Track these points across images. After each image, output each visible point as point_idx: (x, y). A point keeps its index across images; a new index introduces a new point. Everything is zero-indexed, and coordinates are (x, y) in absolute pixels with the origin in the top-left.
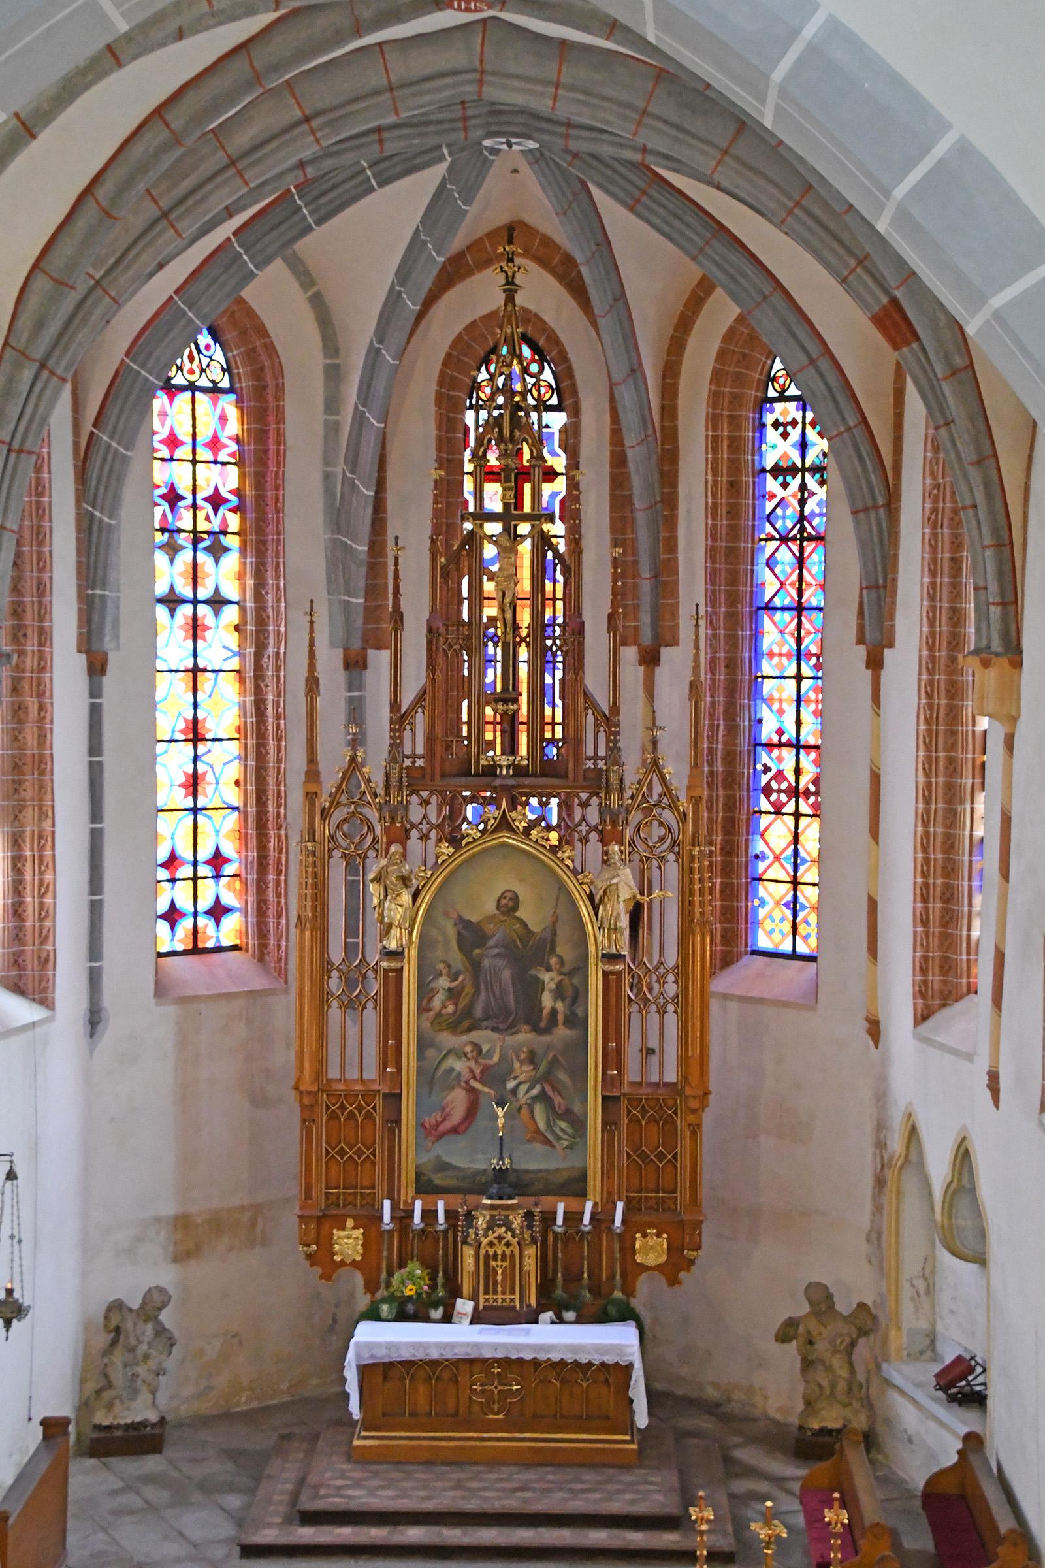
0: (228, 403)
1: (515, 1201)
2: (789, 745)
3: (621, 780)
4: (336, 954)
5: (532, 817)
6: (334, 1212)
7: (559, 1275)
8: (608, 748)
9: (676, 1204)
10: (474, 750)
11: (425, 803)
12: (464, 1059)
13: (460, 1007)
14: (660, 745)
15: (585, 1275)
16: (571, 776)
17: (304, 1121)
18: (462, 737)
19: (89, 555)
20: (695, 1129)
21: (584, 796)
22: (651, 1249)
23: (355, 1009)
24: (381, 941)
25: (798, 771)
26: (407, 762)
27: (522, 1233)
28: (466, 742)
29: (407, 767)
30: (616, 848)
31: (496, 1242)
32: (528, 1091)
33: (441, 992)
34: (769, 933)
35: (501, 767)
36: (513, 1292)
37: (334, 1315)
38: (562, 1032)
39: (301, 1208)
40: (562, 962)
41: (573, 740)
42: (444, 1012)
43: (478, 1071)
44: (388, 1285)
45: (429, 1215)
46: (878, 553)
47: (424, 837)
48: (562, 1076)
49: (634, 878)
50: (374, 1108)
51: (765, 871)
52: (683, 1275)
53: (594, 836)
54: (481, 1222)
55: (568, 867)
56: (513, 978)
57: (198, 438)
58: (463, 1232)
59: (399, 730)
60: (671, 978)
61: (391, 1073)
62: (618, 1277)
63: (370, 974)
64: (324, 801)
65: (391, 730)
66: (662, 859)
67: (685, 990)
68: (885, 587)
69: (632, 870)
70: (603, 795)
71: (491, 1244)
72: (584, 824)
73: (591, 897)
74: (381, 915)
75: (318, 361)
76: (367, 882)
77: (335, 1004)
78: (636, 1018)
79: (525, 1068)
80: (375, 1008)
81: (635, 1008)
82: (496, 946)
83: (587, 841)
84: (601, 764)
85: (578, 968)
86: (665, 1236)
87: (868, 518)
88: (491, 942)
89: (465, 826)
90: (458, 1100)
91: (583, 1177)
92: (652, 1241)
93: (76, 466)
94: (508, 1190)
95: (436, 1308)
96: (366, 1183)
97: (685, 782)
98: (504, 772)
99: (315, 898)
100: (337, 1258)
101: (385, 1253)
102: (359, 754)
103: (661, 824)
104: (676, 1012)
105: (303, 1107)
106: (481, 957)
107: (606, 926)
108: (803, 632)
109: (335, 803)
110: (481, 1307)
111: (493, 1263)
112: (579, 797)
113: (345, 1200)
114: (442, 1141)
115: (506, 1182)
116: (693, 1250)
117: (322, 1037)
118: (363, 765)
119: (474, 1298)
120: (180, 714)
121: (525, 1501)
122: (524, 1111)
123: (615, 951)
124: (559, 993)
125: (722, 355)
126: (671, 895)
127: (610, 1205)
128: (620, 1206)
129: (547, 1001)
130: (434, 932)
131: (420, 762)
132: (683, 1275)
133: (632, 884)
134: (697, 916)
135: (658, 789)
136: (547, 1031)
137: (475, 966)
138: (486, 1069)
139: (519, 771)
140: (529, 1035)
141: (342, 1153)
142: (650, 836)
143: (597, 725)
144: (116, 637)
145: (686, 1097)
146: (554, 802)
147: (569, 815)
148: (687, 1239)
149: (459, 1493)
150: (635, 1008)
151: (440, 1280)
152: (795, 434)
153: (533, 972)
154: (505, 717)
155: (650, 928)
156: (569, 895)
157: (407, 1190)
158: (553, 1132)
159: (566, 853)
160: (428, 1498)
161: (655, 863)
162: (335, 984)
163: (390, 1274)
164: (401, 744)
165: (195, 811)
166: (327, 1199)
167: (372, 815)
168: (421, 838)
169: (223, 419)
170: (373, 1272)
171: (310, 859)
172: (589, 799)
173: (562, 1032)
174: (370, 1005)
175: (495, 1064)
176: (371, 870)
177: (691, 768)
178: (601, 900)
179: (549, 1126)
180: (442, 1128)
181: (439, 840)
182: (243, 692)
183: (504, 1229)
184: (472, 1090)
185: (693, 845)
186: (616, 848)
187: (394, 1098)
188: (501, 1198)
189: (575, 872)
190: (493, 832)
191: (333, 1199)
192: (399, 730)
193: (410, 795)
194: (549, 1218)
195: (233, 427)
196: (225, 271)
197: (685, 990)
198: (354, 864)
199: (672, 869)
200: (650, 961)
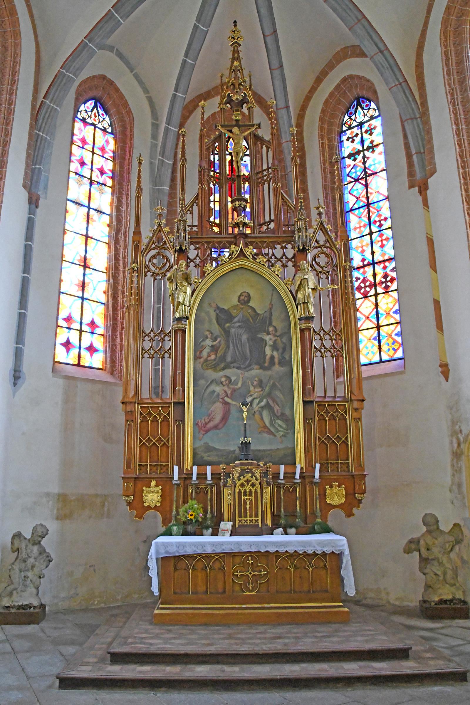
0: (110, 138)
2: (369, 264)
9: (348, 467)
12: (221, 385)
17: (127, 421)
19: (35, 151)
20: (358, 420)
25: (374, 275)
32: (258, 404)
34: (366, 355)
36: (257, 516)
38: (277, 368)
39: (124, 474)
40: (276, 329)
42: (209, 358)
45: (202, 476)
46: (419, 138)
48: (278, 394)
50: (168, 414)
51: (361, 326)
52: (355, 510)
53: (290, 264)
56: (248, 340)
57: (96, 145)
58: (224, 479)
68: (424, 153)
71: (242, 485)
75: (149, 120)
79: (257, 390)
82: (238, 322)
85: (285, 333)
86: (343, 486)
87: (413, 122)
88: (236, 320)
90: (218, 409)
93: (32, 114)
100: (146, 505)
106: (230, 327)
108: (371, 213)
109: (148, 248)
110: (237, 526)
111: (243, 498)
119: (233, 520)
120: (78, 253)
121: (286, 645)
122: (257, 416)
124: (275, 347)
125: (323, 111)
127: (310, 468)
129: (268, 351)
131: (195, 229)
137: (227, 333)
138: (234, 390)
140: (258, 371)
141: (149, 440)
144: (46, 187)
149: (233, 641)
152: (358, 139)
153: (259, 336)
158: (274, 426)
160: (210, 645)
165: (83, 299)
166: (140, 470)
169: (107, 142)
173: (277, 368)
175: (239, 388)
180: (208, 426)
182: (109, 252)
184: (226, 403)
187: (181, 404)
194: (276, 476)
195: (112, 146)
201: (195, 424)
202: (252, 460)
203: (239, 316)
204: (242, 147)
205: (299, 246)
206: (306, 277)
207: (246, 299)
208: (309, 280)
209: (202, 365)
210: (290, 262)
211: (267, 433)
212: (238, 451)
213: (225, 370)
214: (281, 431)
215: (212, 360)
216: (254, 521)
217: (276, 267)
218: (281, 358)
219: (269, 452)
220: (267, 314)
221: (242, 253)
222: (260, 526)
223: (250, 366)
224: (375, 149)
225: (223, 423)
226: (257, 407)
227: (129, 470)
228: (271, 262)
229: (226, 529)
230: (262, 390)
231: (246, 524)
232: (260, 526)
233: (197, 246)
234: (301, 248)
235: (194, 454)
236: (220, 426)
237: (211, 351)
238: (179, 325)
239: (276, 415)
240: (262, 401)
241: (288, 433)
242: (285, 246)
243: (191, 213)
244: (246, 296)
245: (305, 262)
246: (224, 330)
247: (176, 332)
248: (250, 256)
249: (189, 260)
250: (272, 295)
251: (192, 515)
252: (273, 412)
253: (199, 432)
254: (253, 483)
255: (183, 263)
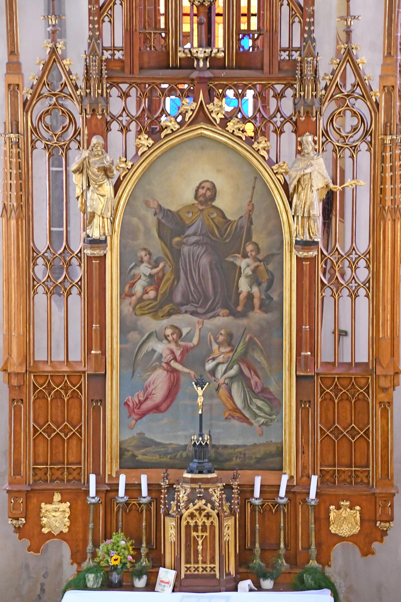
1: (214, 475)
3: (316, 71)
4: (41, 242)
5: (229, 109)
6: (41, 487)
7: (257, 545)
8: (303, 39)
9: (368, 477)
10: (171, 42)
11: (125, 95)
12: (165, 341)
13: (161, 292)
14: (353, 35)
15: (282, 545)
16: (266, 68)
18: (160, 29)
21: (279, 88)
22: (345, 521)
23: (60, 295)
24: (84, 230)
26: (107, 55)
27: (221, 505)
28: (163, 35)
29: (107, 60)
30: (310, 138)
31: (197, 513)
33: (143, 277)
35: (198, 59)
36: (213, 561)
37: (42, 585)
39: (10, 484)
40: (258, 250)
41: (268, 31)
42: (145, 297)
43: (178, 353)
44: (94, 555)
45: (133, 488)
47: (125, 129)
48: (258, 356)
49: (327, 168)
50: (80, 388)
52: (376, 545)
53: (288, 127)
54: (183, 496)
55: (263, 157)
56: (210, 264)
58: (165, 504)
59: (98, 22)
60: (362, 263)
61: (96, 355)
62: (313, 547)
63: (75, 261)
64: (26, 92)
65: (90, 29)
66: (355, 148)
67: (376, 275)
69: (325, 160)
70: (297, 86)
71: (192, 516)
72: (279, 115)
73: (285, 186)
74: (84, 204)
76: (71, 173)
77: (41, 290)
78: (329, 302)
79: (223, 350)
80: (80, 294)
81: (328, 292)
82: (195, 234)
83: (281, 132)
84: (296, 55)
86: (358, 508)
88: (190, 231)
89: (163, 118)
90: (159, 381)
91: (280, 453)
92: (345, 513)
94: (208, 465)
95: (140, 577)
96: (72, 459)
97: (378, 72)
98: (201, 64)
99: (20, 188)
100: (45, 530)
101: (91, 525)
102: (59, 46)
103: (354, 114)
104: (367, 296)
105: (11, 388)
106: (181, 244)
107: (300, 214)
109: (37, 95)
110: (183, 576)
111: (194, 534)
112: (274, 89)
113: (52, 475)
114: (145, 419)
115: (204, 457)
116: (386, 522)
117: (29, 321)
118: (64, 58)
119: (176, 567)
123: (308, 239)
124: (255, 279)
126: (362, 183)
127: (305, 479)
128: (314, 479)
129: (244, 286)
130: (135, 220)
131: (119, 55)
132: (376, 545)
133: (325, 173)
134: (388, 203)
135: (351, 79)
136: (243, 315)
138: (186, 350)
139: (215, 63)
140: (226, 319)
141: (49, 430)
142: (343, 126)
143: (292, 16)
145: (378, 377)
146: (250, 93)
147: (264, 107)
148: (380, 511)
150: (328, 292)
151: (144, 551)
153: (230, 259)
154: (202, 9)
155: (342, 216)
156: (265, 184)
157: (112, 466)
158: (250, 409)
159: (261, 144)
161: (347, 153)
162: (40, 270)
163: (96, 545)
164: (100, 36)
166: (35, 475)
167: (74, 107)
168: (121, 130)
170: (79, 543)
171: (14, 151)
172: (283, 91)
173: (257, 315)
174: (75, 290)
175: (194, 347)
176: (74, 161)
177: (385, 57)
178: (296, 189)
179: (247, 405)
180: (145, 406)
181: (139, 132)
183: (204, 501)
184: (173, 371)
185: (385, 134)
186: (310, 138)
188: (201, 472)
189: (270, 163)
190: (191, 124)
191: (40, 474)
192: (98, 22)
193: (111, 86)
197: (376, 275)
198: (57, 154)
199: (364, 158)
200: (343, 249)
203: (197, 223)
209: (134, 308)
211: (239, 419)
214: (260, 416)
215: (149, 299)
216: (208, 569)
218: (264, 297)
220: (245, 222)
222: (218, 576)
223: (214, 310)
224: (186, 569)
226: (223, 378)
227: (18, 477)
229: (167, 581)
230: (232, 350)
231: (196, 572)
232: (218, 576)
237: (150, 284)
239: (253, 392)
240: (232, 368)
243: (110, 21)
244: (208, 189)
246: (170, 248)
250: (254, 188)
251: (115, 560)
252: (250, 387)
253: (130, 416)
254: (208, 513)
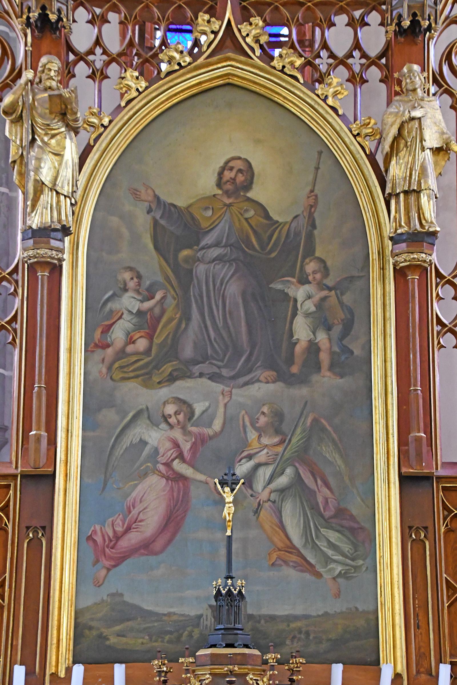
12: (163, 426)
13: (157, 341)
38: (326, 381)
40: (326, 271)
42: (130, 349)
43: (186, 447)
53: (374, 74)
56: (244, 294)
73: (371, 158)
79: (265, 441)
82: (217, 244)
85: (351, 279)
88: (208, 240)
90: (151, 497)
124: (321, 320)
127: (424, 677)
129: (302, 330)
136: (302, 380)
138: (201, 441)
153: (278, 286)
158: (315, 547)
173: (326, 381)
175: (216, 435)
184: (180, 478)
196: (67, 169)
201: (86, 539)
202: (246, 646)
204: (253, 646)
205: (400, 16)
206: (417, 113)
207: (241, 178)
208: (427, 123)
210: (373, 68)
212: (209, 620)
213: (178, 383)
214: (335, 561)
215: (137, 353)
217: (330, 84)
219: (299, 624)
220: (303, 222)
221: (229, 42)
223: (250, 371)
225: (166, 536)
226: (267, 491)
228: (315, 68)
230: (282, 442)
233: (98, 11)
234: (406, 23)
235: (79, 630)
236: (158, 545)
237: (138, 327)
238: (41, 252)
239: (322, 516)
241: (356, 568)
242: (362, 17)
244: (240, 171)
245: (416, 67)
246: (176, 268)
247: (32, 268)
248: (253, 50)
249: (72, 57)
250: (317, 169)
252: (314, 507)
253: (96, 562)
255: (51, 63)
